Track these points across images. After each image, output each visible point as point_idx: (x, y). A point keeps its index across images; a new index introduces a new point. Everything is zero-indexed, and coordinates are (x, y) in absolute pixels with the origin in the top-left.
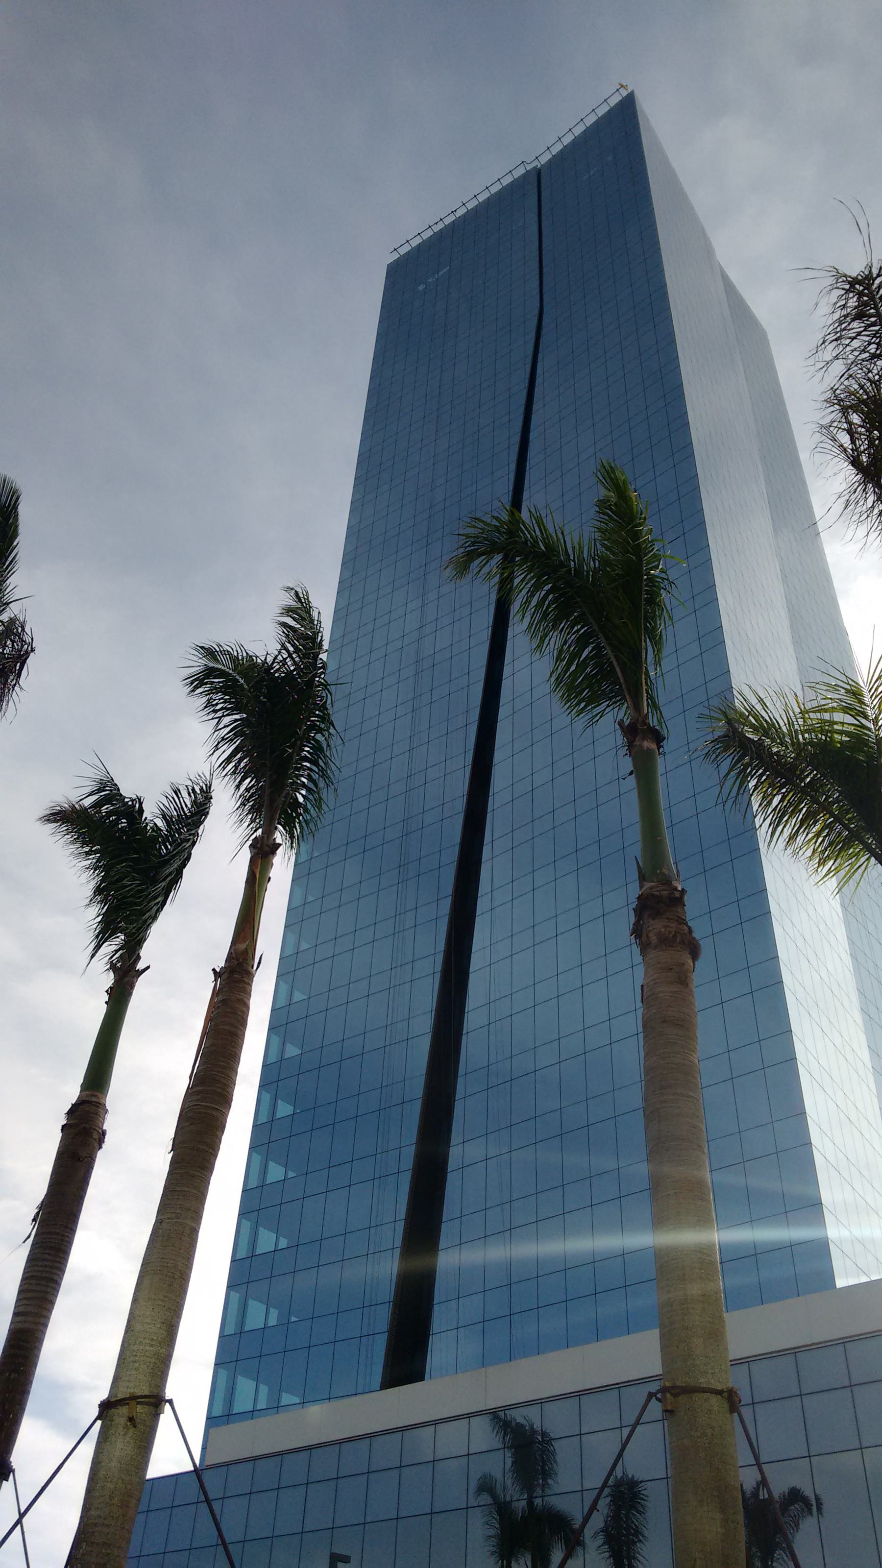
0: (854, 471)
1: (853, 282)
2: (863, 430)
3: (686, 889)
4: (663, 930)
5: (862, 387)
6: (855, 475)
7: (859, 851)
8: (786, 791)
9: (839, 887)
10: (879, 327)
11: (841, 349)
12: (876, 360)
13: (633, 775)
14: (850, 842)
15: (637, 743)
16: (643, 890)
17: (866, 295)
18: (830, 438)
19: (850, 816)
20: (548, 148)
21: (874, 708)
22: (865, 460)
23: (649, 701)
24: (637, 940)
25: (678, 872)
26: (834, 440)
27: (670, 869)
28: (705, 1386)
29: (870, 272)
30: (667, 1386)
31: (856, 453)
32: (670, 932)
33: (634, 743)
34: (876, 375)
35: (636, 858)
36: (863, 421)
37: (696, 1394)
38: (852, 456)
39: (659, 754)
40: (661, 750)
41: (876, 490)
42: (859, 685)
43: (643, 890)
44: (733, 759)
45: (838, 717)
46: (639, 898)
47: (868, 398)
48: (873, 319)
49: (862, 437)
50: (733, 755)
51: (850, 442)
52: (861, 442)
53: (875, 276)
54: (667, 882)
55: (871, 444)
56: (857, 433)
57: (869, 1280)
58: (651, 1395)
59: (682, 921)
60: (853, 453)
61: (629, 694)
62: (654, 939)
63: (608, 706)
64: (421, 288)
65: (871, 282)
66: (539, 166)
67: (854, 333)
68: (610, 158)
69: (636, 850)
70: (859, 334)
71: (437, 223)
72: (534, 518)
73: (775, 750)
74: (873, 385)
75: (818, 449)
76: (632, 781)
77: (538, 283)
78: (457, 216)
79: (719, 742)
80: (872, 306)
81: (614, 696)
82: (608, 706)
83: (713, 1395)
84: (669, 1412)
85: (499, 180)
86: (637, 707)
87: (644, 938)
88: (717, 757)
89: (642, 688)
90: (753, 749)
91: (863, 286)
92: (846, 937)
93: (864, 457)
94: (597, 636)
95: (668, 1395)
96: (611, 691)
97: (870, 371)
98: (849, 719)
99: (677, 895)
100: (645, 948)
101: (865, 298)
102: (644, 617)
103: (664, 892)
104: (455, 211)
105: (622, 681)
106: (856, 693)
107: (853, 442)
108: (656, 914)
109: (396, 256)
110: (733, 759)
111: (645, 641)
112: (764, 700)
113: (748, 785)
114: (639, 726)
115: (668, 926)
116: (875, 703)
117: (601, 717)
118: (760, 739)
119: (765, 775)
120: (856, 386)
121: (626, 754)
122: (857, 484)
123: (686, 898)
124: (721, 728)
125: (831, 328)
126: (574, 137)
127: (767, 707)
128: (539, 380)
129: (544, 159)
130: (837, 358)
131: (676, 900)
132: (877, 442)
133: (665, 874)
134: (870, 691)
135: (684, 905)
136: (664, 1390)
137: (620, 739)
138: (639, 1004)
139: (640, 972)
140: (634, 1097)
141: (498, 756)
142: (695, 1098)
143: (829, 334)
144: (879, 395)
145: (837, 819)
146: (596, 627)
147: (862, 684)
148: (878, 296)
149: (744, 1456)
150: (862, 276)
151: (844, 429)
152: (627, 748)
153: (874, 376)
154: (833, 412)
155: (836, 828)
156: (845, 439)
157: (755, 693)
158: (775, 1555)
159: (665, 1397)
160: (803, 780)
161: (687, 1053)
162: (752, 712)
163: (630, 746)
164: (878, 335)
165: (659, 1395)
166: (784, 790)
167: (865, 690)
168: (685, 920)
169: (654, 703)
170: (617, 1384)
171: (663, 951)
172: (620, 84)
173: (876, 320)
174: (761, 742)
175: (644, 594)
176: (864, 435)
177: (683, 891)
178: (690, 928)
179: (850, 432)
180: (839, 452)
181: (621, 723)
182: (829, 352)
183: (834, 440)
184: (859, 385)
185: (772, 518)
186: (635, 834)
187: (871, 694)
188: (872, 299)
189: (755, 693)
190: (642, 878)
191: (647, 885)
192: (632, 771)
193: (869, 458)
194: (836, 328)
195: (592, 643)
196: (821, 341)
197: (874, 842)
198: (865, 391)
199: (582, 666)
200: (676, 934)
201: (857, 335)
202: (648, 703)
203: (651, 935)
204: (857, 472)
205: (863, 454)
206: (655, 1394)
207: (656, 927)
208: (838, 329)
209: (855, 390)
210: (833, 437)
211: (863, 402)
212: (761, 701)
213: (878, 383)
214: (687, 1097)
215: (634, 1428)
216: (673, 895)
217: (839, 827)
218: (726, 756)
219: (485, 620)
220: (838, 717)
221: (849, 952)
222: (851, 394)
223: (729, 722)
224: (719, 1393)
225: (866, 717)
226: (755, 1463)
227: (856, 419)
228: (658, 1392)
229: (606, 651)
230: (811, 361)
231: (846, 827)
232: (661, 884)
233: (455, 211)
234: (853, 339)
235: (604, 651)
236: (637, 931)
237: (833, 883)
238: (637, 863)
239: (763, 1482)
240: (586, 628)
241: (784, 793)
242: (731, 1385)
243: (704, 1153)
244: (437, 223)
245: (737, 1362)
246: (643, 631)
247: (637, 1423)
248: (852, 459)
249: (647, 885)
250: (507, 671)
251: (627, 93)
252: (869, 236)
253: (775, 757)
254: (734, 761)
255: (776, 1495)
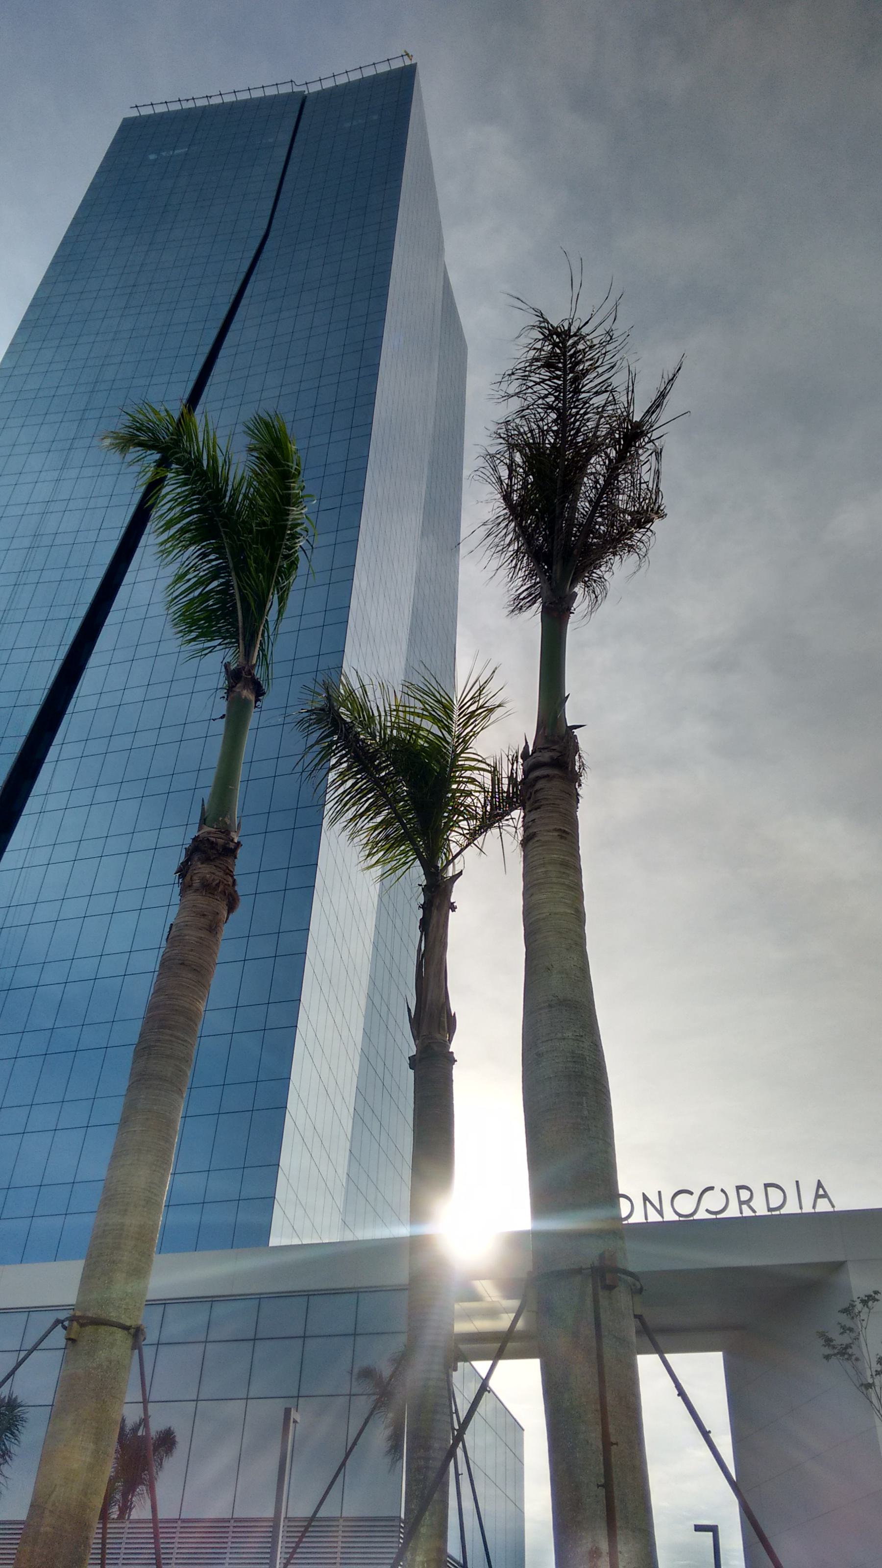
0: (502, 505)
1: (553, 331)
2: (521, 470)
3: (242, 843)
4: (208, 876)
5: (531, 431)
6: (502, 509)
7: (408, 851)
8: (361, 778)
9: (382, 878)
10: (562, 382)
11: (524, 388)
12: (550, 411)
13: (224, 719)
14: (401, 841)
15: (237, 689)
16: (200, 833)
17: (559, 348)
18: (492, 466)
19: (411, 816)
20: (320, 80)
21: (459, 725)
22: (515, 498)
23: (261, 653)
24: (180, 880)
25: (239, 824)
26: (495, 469)
27: (232, 819)
28: (114, 1320)
29: (569, 329)
30: (77, 1315)
31: (509, 489)
32: (214, 880)
33: (234, 689)
34: (546, 425)
35: (203, 801)
36: (524, 462)
37: (103, 1327)
38: (505, 491)
39: (256, 707)
40: (258, 703)
41: (517, 528)
42: (453, 702)
43: (200, 833)
44: (323, 732)
45: (427, 724)
46: (195, 839)
47: (534, 443)
48: (558, 373)
49: (519, 476)
50: (324, 729)
51: (507, 477)
52: (516, 482)
53: (572, 334)
54: (226, 831)
55: (525, 487)
56: (516, 471)
57: (300, 1243)
58: (58, 1322)
59: (230, 873)
60: (507, 488)
61: (244, 639)
62: (197, 883)
63: (220, 644)
64: (152, 157)
65: (567, 338)
66: (306, 92)
67: (539, 378)
68: (375, 117)
69: (206, 794)
70: (543, 381)
71: (188, 100)
72: (253, 578)
73: (362, 737)
74: (541, 434)
75: (479, 473)
76: (221, 725)
77: (271, 206)
78: (211, 103)
79: (315, 713)
80: (562, 361)
81: (230, 636)
82: (220, 644)
83: (120, 1330)
84: (71, 1340)
85: (263, 87)
86: (248, 654)
87: (188, 878)
88: (308, 727)
89: (257, 638)
90: (344, 729)
91: (559, 339)
92: (374, 927)
93: (515, 495)
94: (229, 572)
95: (75, 1323)
96: (227, 631)
97: (542, 419)
98: (435, 730)
99: (232, 846)
100: (185, 889)
101: (558, 351)
102: (278, 570)
103: (219, 840)
104: (211, 97)
105: (240, 624)
106: (447, 709)
107: (510, 478)
108: (207, 860)
109: (134, 113)
110: (323, 732)
111: (273, 594)
112: (366, 686)
113: (330, 760)
114: (244, 674)
115: (214, 873)
116: (461, 721)
117: (210, 652)
118: (352, 722)
119: (346, 757)
120: (526, 429)
121: (224, 697)
122: (502, 518)
123: (239, 851)
124: (320, 702)
125: (522, 365)
126: (348, 81)
127: (367, 695)
128: (244, 302)
129: (314, 88)
130: (517, 394)
131: (230, 851)
132: (529, 486)
133: (226, 823)
134: (460, 709)
135: (236, 858)
136: (72, 1319)
137: (223, 682)
138: (164, 943)
139: (175, 910)
140: (132, 1032)
141: (95, 660)
142: (189, 1042)
143: (520, 369)
144: (543, 444)
145: (399, 818)
146: (231, 566)
147: (455, 702)
148: (569, 354)
149: (133, 1393)
150: (561, 330)
151: (506, 464)
152: (226, 691)
153: (543, 426)
154: (501, 444)
155: (395, 824)
156: (504, 473)
157: (360, 680)
158: (138, 1490)
159: (71, 1325)
160: (380, 771)
161: (196, 1000)
162: (351, 693)
163: (230, 689)
164: (558, 389)
165: (66, 1323)
166: (359, 776)
167: (456, 707)
168: (232, 872)
169: (265, 656)
170: (28, 1308)
171: (202, 896)
172: (405, 52)
173: (561, 375)
174: (352, 725)
175: (284, 548)
176: (521, 475)
177: (238, 844)
178: (234, 881)
179: (511, 468)
180: (494, 481)
181: (227, 666)
182: (514, 387)
183: (495, 469)
184: (529, 428)
185: (423, 522)
186: (209, 779)
187: (459, 723)
188: (564, 354)
189: (360, 680)
190: (203, 821)
191: (206, 829)
192: (224, 715)
193: (519, 498)
194: (526, 367)
195: (222, 578)
196: (510, 372)
197: (423, 846)
198: (532, 435)
199: (205, 597)
200: (219, 882)
201: (541, 382)
202: (259, 655)
203: (195, 878)
204: (505, 507)
205: (515, 493)
206: (62, 1322)
207: (203, 870)
208: (528, 369)
209: (525, 432)
210: (494, 467)
211: (528, 444)
212: (363, 687)
213: (545, 432)
214: (182, 1040)
215: (30, 1352)
216: (227, 845)
217: (397, 824)
218: (317, 728)
219: (123, 518)
220: (427, 724)
221: (372, 940)
222: (520, 434)
223: (329, 698)
224: (126, 1328)
225: (450, 732)
226: (142, 1401)
227: (518, 458)
228: (67, 1319)
229: (232, 591)
230: (495, 387)
231: (404, 826)
232: (220, 831)
233: (211, 97)
234: (537, 383)
235: (231, 590)
236: (183, 871)
237: (378, 871)
238: (203, 805)
239: (145, 1421)
240: (221, 561)
241: (358, 779)
242: (140, 1323)
243: (182, 1097)
244: (188, 100)
245: (152, 1303)
246: (273, 583)
247: (35, 1348)
248: (505, 493)
249: (206, 829)
250: (128, 578)
251: (410, 63)
252: (578, 295)
253: (361, 743)
254: (323, 735)
255: (153, 1433)
